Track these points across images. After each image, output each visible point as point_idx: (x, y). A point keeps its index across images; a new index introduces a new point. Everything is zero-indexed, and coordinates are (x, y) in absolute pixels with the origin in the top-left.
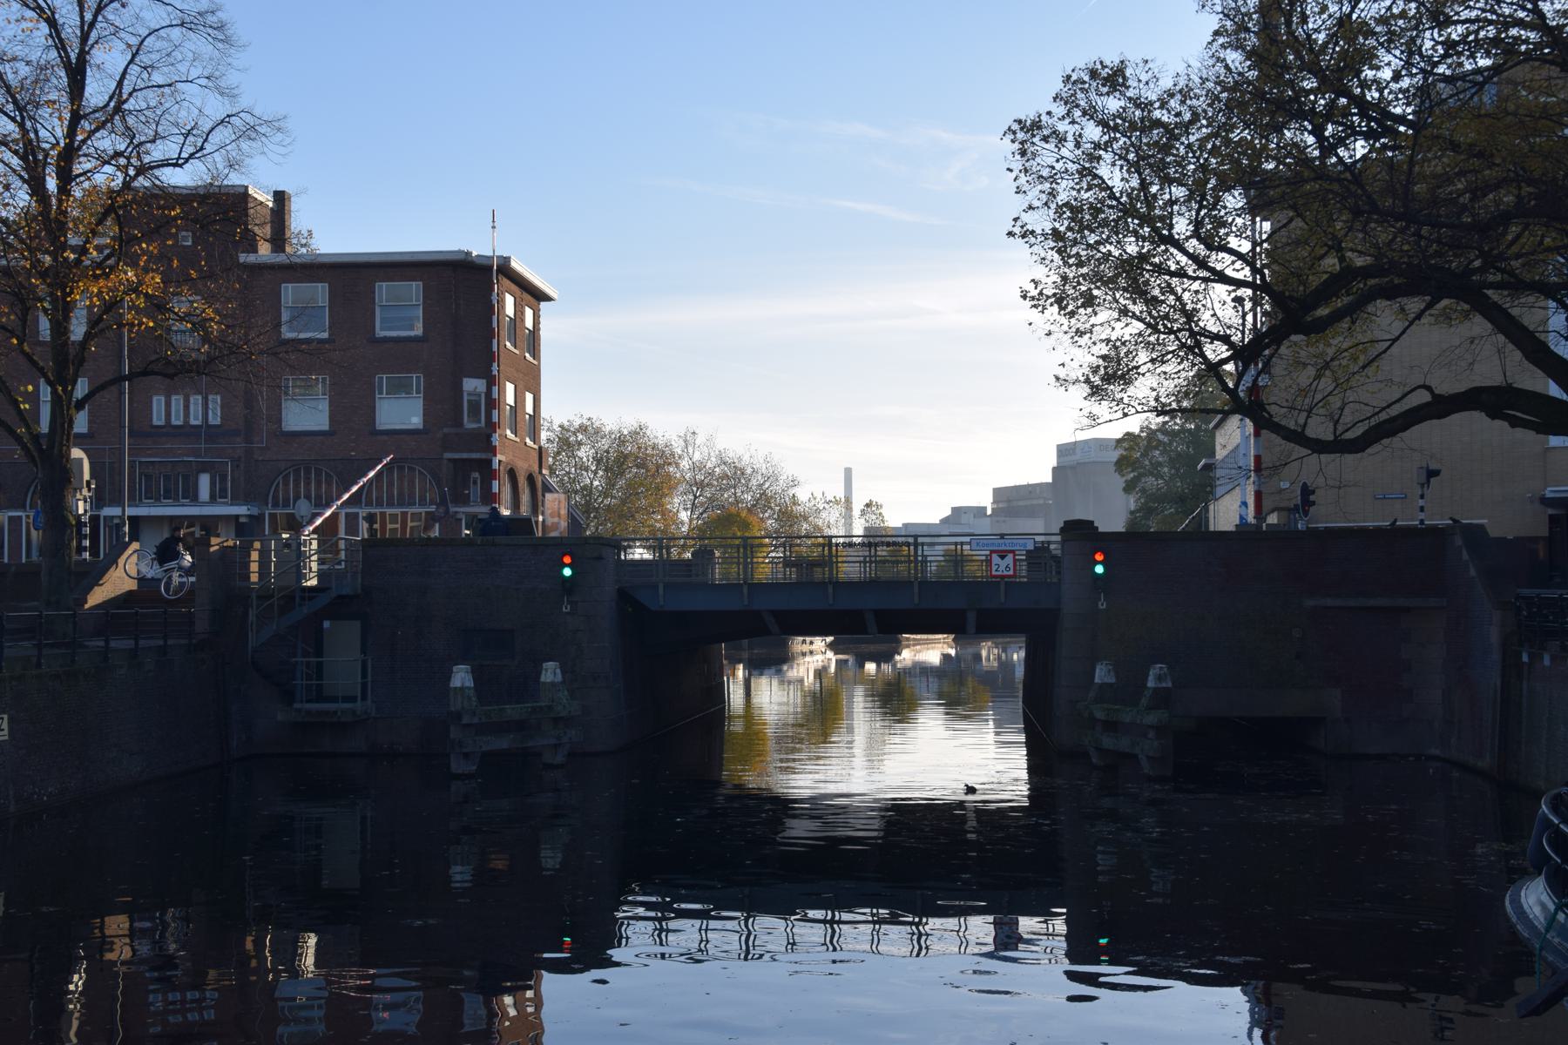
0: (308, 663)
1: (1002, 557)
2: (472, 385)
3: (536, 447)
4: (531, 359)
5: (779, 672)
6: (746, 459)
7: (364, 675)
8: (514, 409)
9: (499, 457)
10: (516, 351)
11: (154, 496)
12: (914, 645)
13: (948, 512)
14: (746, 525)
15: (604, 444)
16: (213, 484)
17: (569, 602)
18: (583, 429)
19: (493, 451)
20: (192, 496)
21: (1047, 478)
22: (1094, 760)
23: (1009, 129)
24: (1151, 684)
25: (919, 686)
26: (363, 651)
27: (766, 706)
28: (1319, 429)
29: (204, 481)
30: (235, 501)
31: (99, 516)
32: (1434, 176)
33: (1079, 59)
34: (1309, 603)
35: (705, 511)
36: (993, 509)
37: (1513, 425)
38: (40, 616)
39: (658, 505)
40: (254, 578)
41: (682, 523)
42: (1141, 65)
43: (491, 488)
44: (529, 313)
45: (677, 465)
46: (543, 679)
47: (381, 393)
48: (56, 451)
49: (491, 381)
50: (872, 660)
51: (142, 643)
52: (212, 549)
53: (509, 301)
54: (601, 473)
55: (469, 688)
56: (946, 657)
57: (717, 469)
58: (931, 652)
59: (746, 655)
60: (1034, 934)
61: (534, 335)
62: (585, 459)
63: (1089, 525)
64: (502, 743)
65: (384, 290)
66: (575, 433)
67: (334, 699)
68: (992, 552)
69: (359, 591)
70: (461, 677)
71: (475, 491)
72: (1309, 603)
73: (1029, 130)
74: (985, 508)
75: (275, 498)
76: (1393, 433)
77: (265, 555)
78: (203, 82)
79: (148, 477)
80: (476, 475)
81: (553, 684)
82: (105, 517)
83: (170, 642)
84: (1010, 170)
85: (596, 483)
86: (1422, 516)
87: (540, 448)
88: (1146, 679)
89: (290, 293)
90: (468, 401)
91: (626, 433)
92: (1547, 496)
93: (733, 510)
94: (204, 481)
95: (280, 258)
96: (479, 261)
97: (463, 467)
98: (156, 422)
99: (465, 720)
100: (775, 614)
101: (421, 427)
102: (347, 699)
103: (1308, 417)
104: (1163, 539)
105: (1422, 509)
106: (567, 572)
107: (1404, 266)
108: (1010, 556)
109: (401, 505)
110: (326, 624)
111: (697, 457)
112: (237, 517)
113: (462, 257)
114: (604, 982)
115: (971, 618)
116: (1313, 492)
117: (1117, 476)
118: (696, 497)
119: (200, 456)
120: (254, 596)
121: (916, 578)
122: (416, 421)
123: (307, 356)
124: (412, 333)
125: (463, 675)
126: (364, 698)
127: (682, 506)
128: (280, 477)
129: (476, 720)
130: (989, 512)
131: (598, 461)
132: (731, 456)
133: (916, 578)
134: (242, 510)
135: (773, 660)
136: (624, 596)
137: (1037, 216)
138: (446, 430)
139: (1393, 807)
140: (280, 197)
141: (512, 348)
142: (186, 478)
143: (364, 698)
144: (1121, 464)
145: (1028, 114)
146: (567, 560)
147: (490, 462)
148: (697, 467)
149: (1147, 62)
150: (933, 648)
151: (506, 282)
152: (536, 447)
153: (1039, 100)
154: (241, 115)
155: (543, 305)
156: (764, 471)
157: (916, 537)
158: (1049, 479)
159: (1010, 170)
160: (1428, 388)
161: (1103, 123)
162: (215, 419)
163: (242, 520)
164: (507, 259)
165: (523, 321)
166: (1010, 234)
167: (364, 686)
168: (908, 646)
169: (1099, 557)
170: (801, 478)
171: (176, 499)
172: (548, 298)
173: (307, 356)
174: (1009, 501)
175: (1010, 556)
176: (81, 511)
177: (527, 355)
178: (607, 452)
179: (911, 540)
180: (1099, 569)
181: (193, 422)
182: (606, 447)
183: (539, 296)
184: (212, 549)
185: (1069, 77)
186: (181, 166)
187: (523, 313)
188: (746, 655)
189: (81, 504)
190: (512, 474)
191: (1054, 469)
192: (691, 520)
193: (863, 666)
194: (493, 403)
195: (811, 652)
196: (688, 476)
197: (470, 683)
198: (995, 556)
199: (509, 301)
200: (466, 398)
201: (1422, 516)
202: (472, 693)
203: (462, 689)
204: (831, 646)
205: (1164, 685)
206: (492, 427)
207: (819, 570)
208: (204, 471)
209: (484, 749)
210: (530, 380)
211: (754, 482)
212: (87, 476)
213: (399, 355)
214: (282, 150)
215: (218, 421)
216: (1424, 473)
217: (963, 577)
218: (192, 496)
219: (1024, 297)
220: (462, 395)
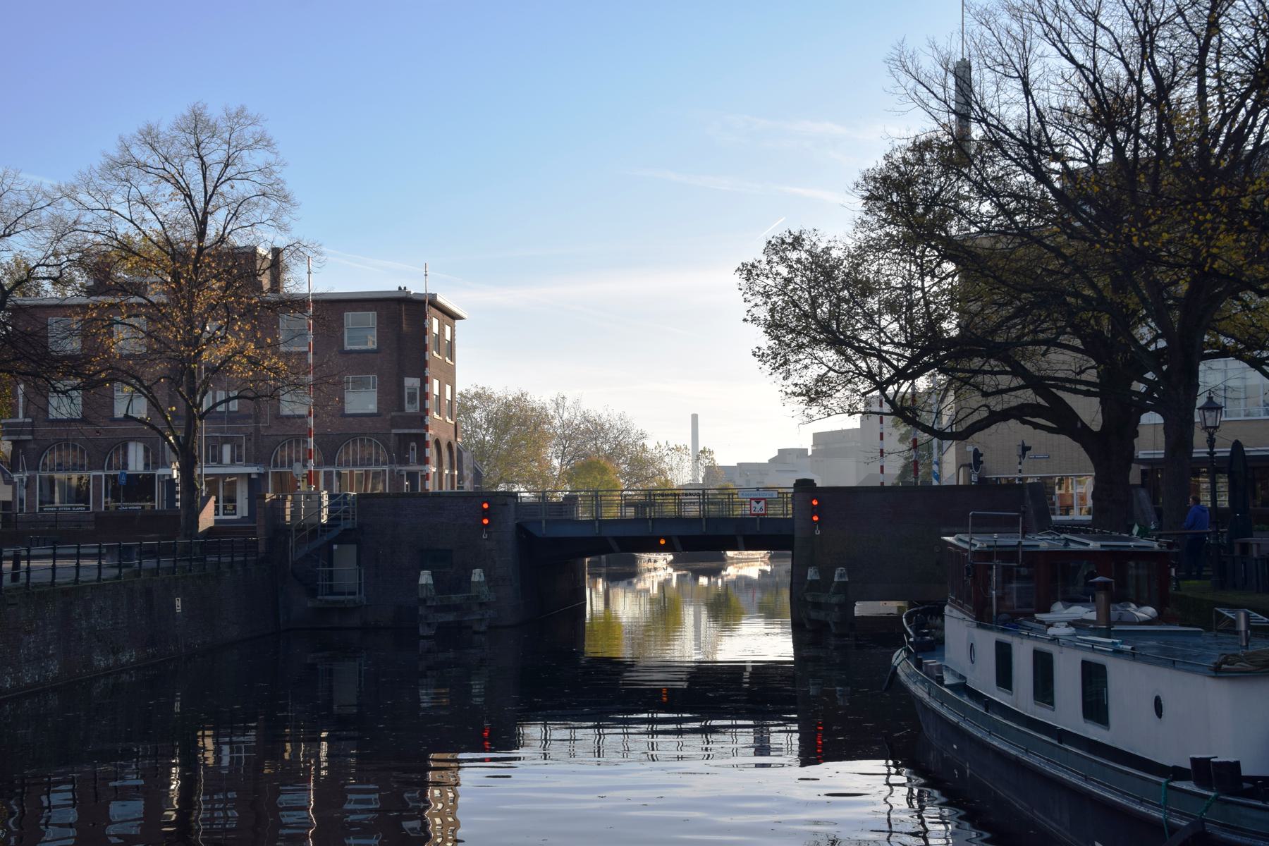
1: (758, 502)
2: (411, 382)
3: (453, 422)
5: (630, 584)
6: (604, 416)
7: (360, 579)
8: (439, 398)
9: (430, 432)
10: (440, 357)
12: (737, 563)
14: (603, 471)
15: (494, 407)
16: (233, 451)
18: (478, 396)
19: (426, 428)
24: (836, 579)
25: (743, 599)
26: (359, 563)
27: (620, 613)
29: (227, 449)
30: (248, 463)
31: (154, 475)
35: (572, 459)
36: (813, 451)
37: (1035, 428)
38: (191, 543)
39: (536, 456)
40: (288, 518)
41: (555, 468)
43: (425, 454)
44: (448, 329)
45: (550, 423)
46: (473, 579)
48: (190, 445)
49: (425, 381)
52: (266, 501)
53: (435, 322)
54: (491, 430)
56: (763, 572)
57: (582, 426)
58: (751, 568)
59: (604, 570)
60: (699, 662)
61: (451, 345)
62: (479, 420)
63: (811, 482)
64: (450, 617)
65: (350, 317)
66: (471, 400)
67: (343, 594)
68: (751, 499)
69: (356, 526)
70: (425, 578)
71: (413, 455)
73: (749, 272)
74: (807, 449)
75: (275, 461)
77: (296, 504)
78: (270, 222)
80: (413, 444)
81: (479, 582)
82: (159, 476)
84: (741, 289)
85: (487, 438)
88: (834, 577)
90: (408, 393)
91: (511, 399)
92: (1140, 457)
93: (595, 456)
94: (227, 449)
97: (404, 440)
101: (376, 411)
102: (350, 594)
107: (135, 750)
108: (763, 502)
109: (362, 465)
110: (335, 547)
111: (566, 416)
112: (249, 475)
115: (740, 540)
116: (982, 455)
118: (565, 448)
120: (293, 529)
121: (650, 516)
122: (372, 407)
125: (426, 576)
126: (360, 593)
127: (554, 455)
129: (434, 604)
130: (810, 453)
131: (489, 422)
132: (593, 415)
133: (650, 516)
134: (253, 470)
135: (625, 574)
136: (520, 528)
138: (393, 414)
140: (276, 252)
143: (360, 593)
145: (749, 260)
147: (423, 436)
148: (567, 424)
150: (752, 565)
151: (433, 310)
153: (755, 253)
155: (457, 322)
156: (619, 427)
157: (704, 490)
159: (741, 289)
163: (253, 476)
164: (435, 296)
165: (444, 335)
166: (745, 320)
167: (360, 584)
168: (732, 564)
170: (648, 432)
172: (460, 318)
175: (763, 502)
177: (447, 359)
178: (496, 414)
179: (701, 492)
182: (495, 410)
183: (454, 317)
184: (266, 501)
185: (770, 242)
187: (444, 330)
188: (604, 570)
190: (437, 442)
192: (562, 465)
193: (697, 579)
194: (425, 396)
195: (655, 569)
196: (559, 431)
197: (430, 581)
198: (753, 502)
199: (435, 322)
200: (406, 391)
202: (432, 587)
203: (426, 585)
204: (671, 564)
205: (843, 580)
206: (425, 411)
208: (226, 443)
209: (440, 620)
211: (611, 435)
214: (320, 265)
219: (754, 355)
220: (404, 391)
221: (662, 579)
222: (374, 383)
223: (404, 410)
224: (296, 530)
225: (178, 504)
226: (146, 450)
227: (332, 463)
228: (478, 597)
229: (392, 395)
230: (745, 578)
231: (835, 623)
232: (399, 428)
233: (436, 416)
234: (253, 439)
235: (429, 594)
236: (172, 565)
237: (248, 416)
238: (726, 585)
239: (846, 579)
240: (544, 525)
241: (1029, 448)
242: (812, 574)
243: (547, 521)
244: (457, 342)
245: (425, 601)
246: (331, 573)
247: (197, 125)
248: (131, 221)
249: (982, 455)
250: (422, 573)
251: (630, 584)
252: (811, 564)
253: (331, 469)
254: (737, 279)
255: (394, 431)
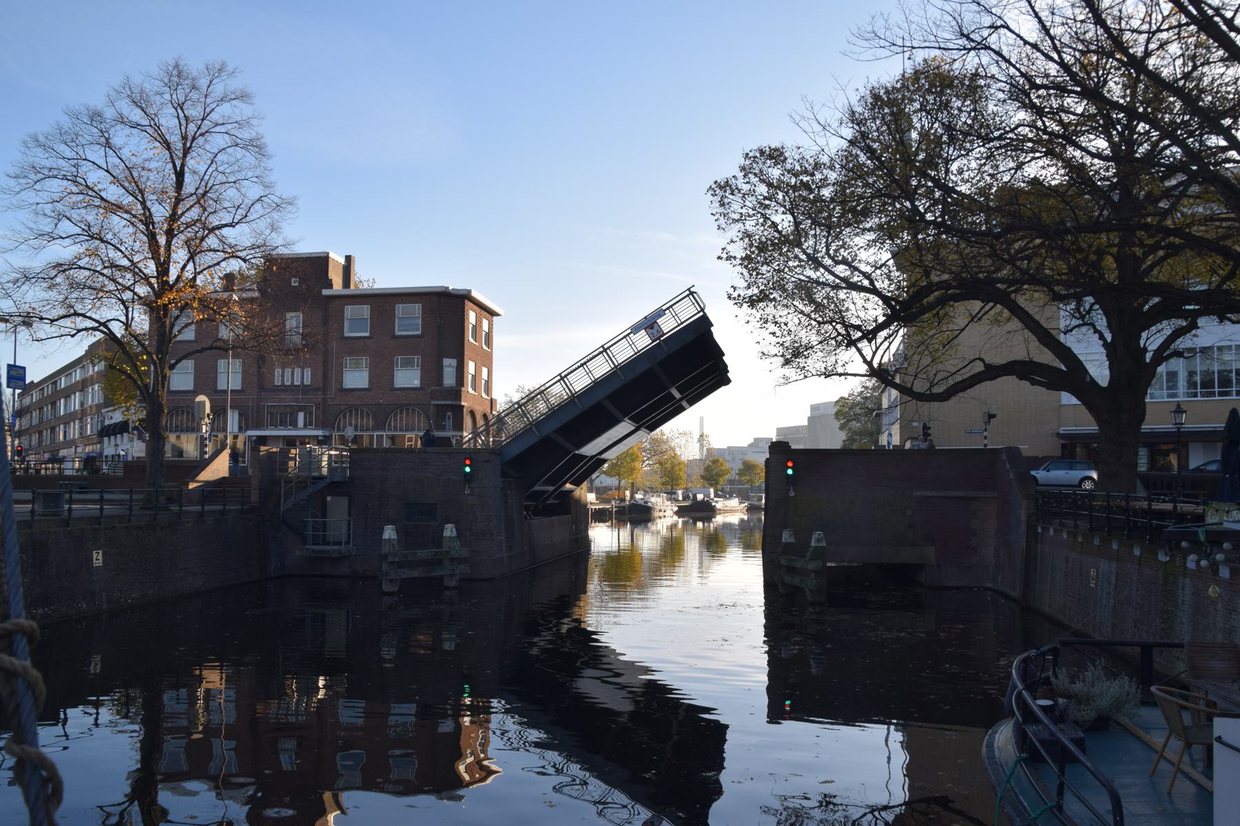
0: (316, 522)
3: (489, 398)
4: (487, 349)
11: (275, 425)
13: (752, 441)
20: (294, 424)
21: (805, 423)
22: (781, 590)
23: (710, 187)
26: (349, 515)
28: (920, 386)
29: (301, 416)
30: (317, 428)
33: (754, 144)
34: (918, 493)
42: (796, 150)
46: (445, 534)
47: (397, 367)
50: (700, 520)
51: (206, 508)
52: (261, 453)
55: (394, 540)
61: (489, 339)
64: (416, 573)
65: (400, 309)
67: (328, 544)
71: (449, 423)
72: (918, 493)
73: (724, 188)
76: (964, 389)
78: (255, 180)
79: (272, 414)
80: (450, 413)
83: (227, 507)
86: (986, 442)
87: (492, 399)
89: (349, 310)
94: (301, 416)
95: (346, 292)
96: (453, 292)
97: (442, 410)
98: (276, 383)
99: (390, 559)
102: (335, 543)
103: (915, 379)
104: (862, 452)
105: (985, 438)
106: (468, 469)
110: (329, 498)
112: (318, 436)
113: (444, 290)
116: (930, 428)
117: (836, 420)
119: (298, 402)
122: (416, 383)
123: (355, 347)
124: (396, 330)
128: (392, 415)
129: (397, 559)
137: (736, 247)
138: (433, 388)
139: (961, 626)
141: (474, 342)
142: (291, 414)
144: (838, 415)
145: (721, 178)
146: (468, 462)
149: (799, 148)
152: (489, 398)
154: (269, 196)
155: (495, 318)
158: (806, 424)
160: (982, 360)
161: (770, 185)
162: (307, 382)
163: (320, 438)
164: (469, 291)
165: (481, 326)
166: (719, 258)
168: (720, 514)
169: (790, 464)
171: (286, 426)
172: (498, 315)
173: (355, 347)
174: (785, 435)
176: (204, 431)
180: (790, 472)
181: (296, 383)
183: (492, 313)
184: (261, 453)
185: (747, 154)
186: (234, 226)
187: (481, 322)
189: (204, 427)
190: (472, 413)
191: (809, 418)
193: (695, 524)
195: (665, 516)
197: (394, 536)
201: (986, 442)
202: (395, 542)
203: (389, 540)
205: (821, 545)
208: (301, 411)
209: (402, 577)
210: (486, 360)
212: (208, 410)
213: (408, 345)
215: (309, 383)
216: (986, 415)
218: (294, 424)
219: (729, 298)
221: (670, 524)
222: (418, 362)
224: (285, 482)
226: (240, 415)
227: (383, 429)
228: (447, 552)
229: (433, 373)
230: (730, 524)
233: (470, 390)
234: (321, 407)
235: (391, 550)
236: (29, 518)
237: (318, 389)
238: (716, 529)
239: (824, 544)
241: (993, 416)
242: (787, 537)
244: (494, 334)
245: (386, 556)
246: (325, 523)
247: (176, 76)
248: (107, 171)
249: (930, 428)
250: (386, 527)
251: (646, 527)
252: (786, 526)
253: (382, 433)
254: (708, 204)
255: (433, 402)
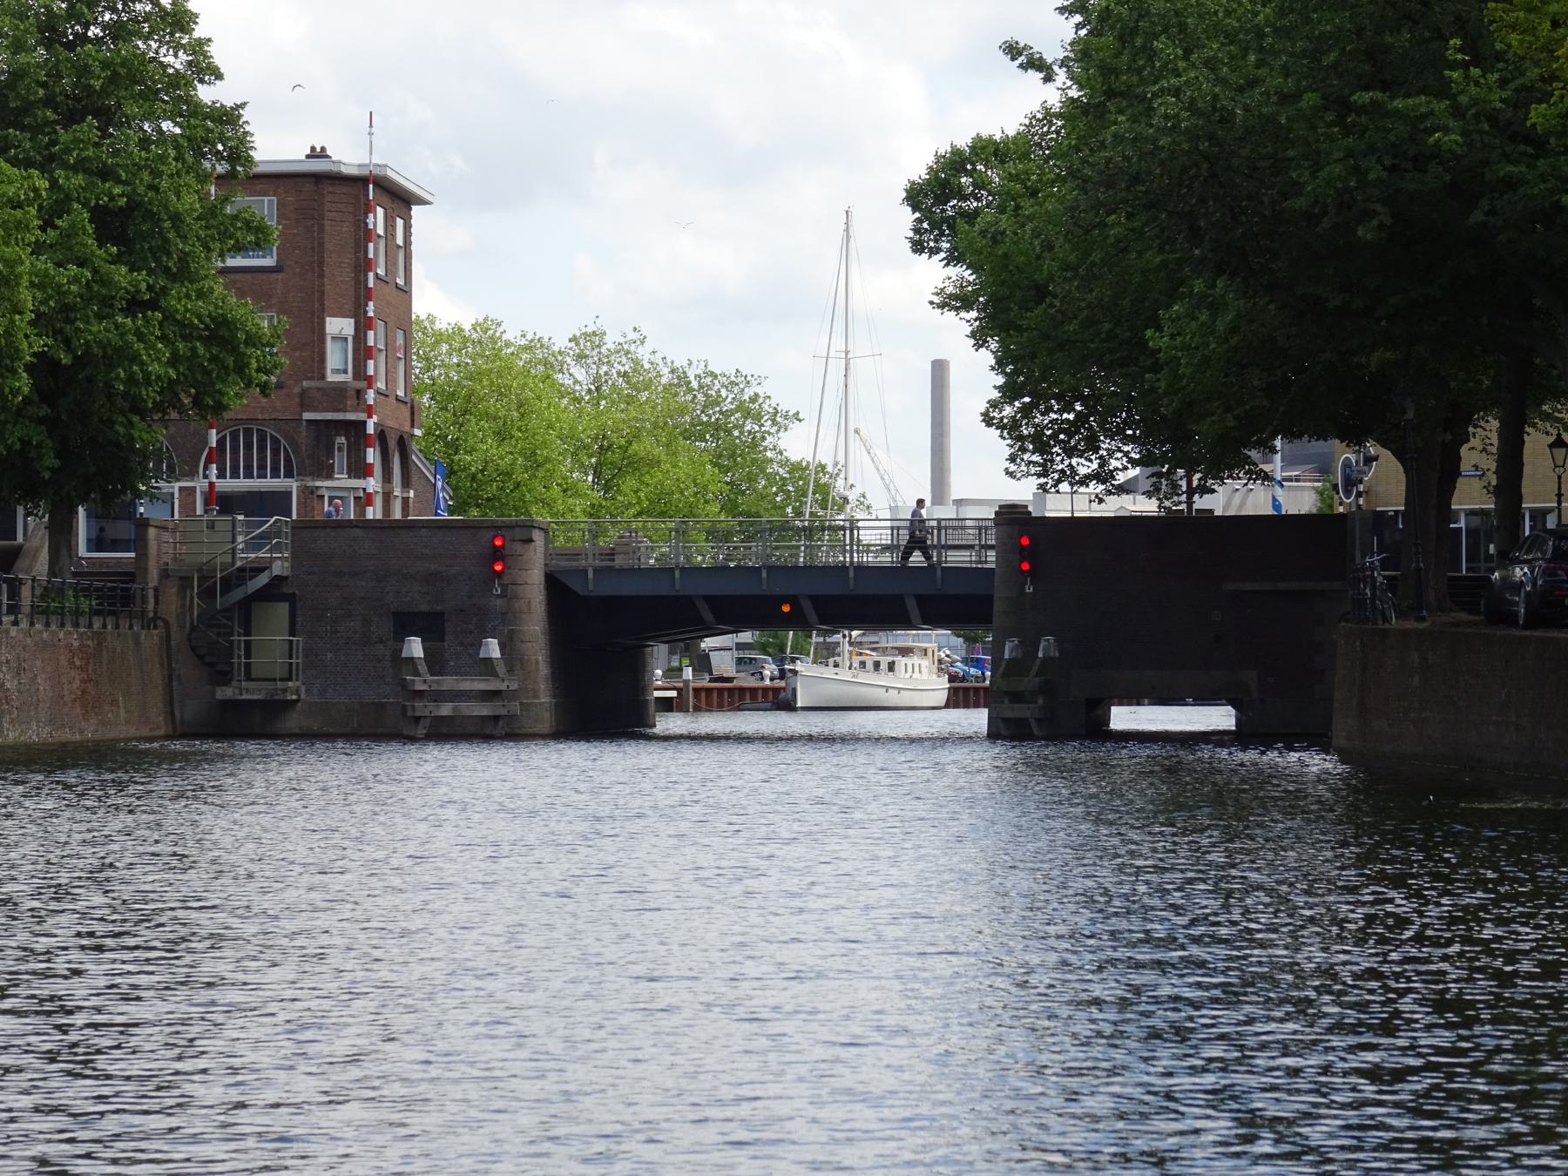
17: (499, 584)
32: (1321, 169)
69: (43, 427)
71: (340, 459)
80: (342, 440)
100: (711, 600)
114: (723, 1134)
121: (852, 562)
133: (852, 562)
138: (305, 384)
187: (394, 227)
207: (989, 543)
217: (946, 562)
223: (323, 376)
225: (1425, 803)
231: (1038, 720)
232: (315, 410)
240: (590, 575)
243: (595, 571)
255: (307, 416)
